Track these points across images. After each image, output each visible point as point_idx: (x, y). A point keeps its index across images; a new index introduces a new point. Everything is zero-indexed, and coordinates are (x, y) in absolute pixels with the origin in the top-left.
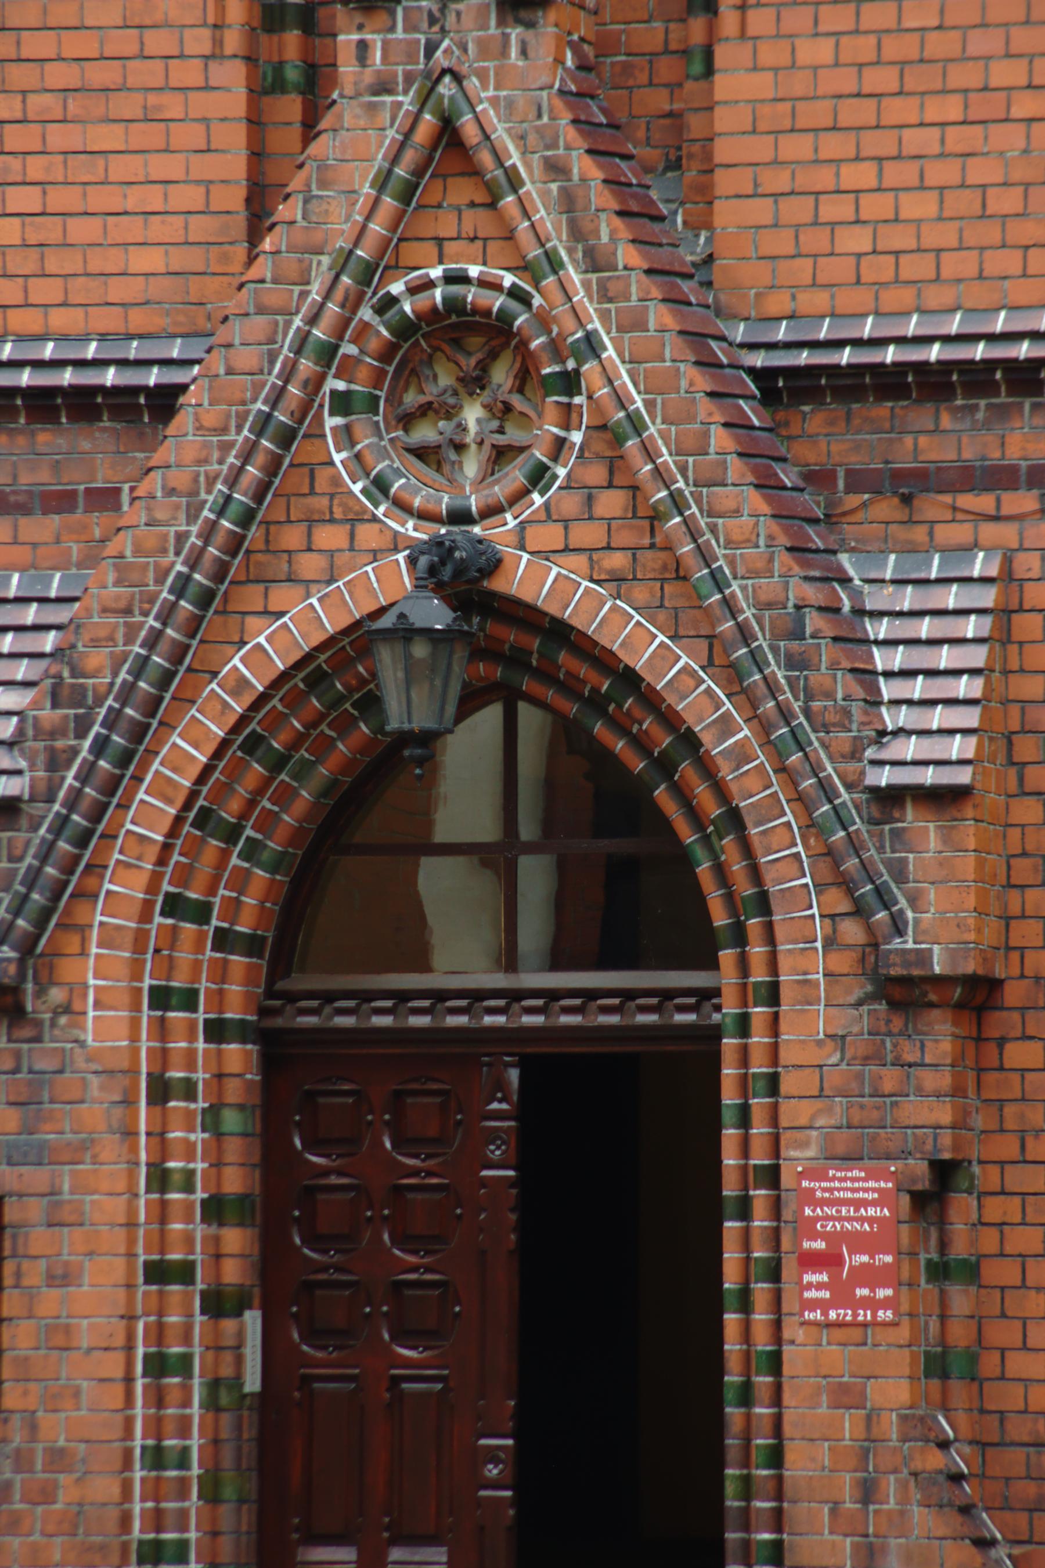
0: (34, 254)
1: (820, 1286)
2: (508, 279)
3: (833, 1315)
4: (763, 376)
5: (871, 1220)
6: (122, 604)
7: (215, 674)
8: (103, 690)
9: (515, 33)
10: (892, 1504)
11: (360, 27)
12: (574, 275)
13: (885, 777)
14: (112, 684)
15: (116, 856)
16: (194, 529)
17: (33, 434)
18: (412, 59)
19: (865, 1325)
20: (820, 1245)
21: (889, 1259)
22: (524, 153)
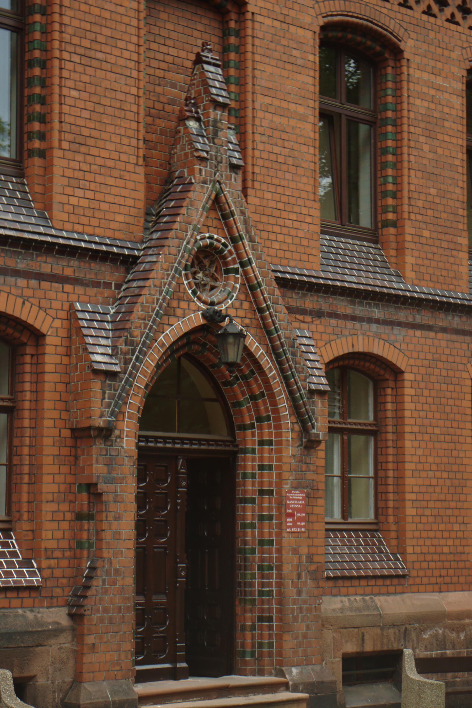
0: (92, 211)
1: (290, 522)
2: (223, 241)
3: (293, 530)
4: (277, 279)
5: (301, 504)
6: (143, 317)
7: (156, 341)
8: (138, 342)
9: (233, 175)
10: (304, 580)
11: (200, 165)
12: (246, 242)
13: (313, 387)
14: (141, 340)
15: (132, 392)
16: (161, 298)
17: (90, 264)
18: (211, 177)
19: (299, 532)
20: (290, 511)
21: (304, 515)
22: (236, 207)
